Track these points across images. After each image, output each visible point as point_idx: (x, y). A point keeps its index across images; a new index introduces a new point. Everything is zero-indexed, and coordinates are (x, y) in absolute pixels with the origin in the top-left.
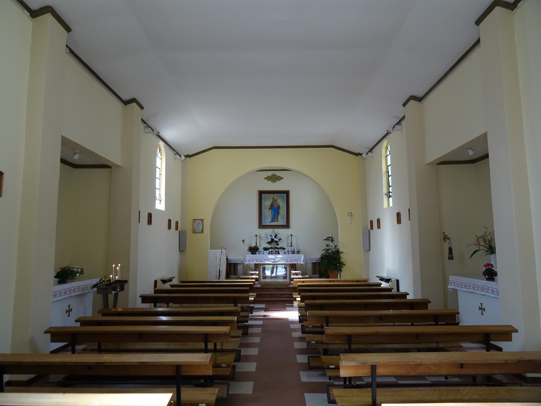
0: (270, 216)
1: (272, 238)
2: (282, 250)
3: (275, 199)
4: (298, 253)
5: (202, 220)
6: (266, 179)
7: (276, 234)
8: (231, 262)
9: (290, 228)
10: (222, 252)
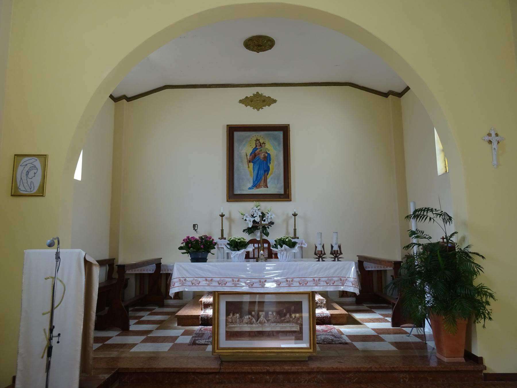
0: (251, 175)
1: (254, 221)
2: (285, 250)
3: (261, 141)
4: (320, 257)
5: (43, 158)
6: (243, 103)
7: (262, 213)
8: (168, 270)
9: (291, 201)
10: (58, 257)
